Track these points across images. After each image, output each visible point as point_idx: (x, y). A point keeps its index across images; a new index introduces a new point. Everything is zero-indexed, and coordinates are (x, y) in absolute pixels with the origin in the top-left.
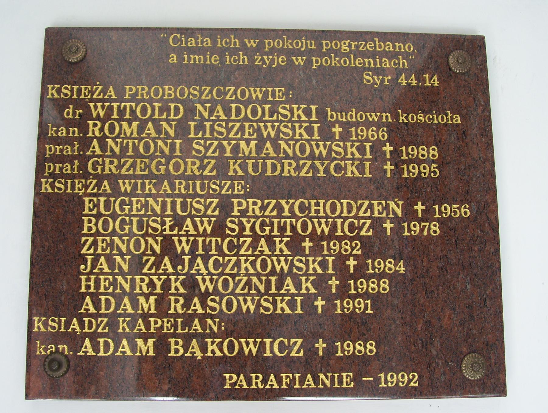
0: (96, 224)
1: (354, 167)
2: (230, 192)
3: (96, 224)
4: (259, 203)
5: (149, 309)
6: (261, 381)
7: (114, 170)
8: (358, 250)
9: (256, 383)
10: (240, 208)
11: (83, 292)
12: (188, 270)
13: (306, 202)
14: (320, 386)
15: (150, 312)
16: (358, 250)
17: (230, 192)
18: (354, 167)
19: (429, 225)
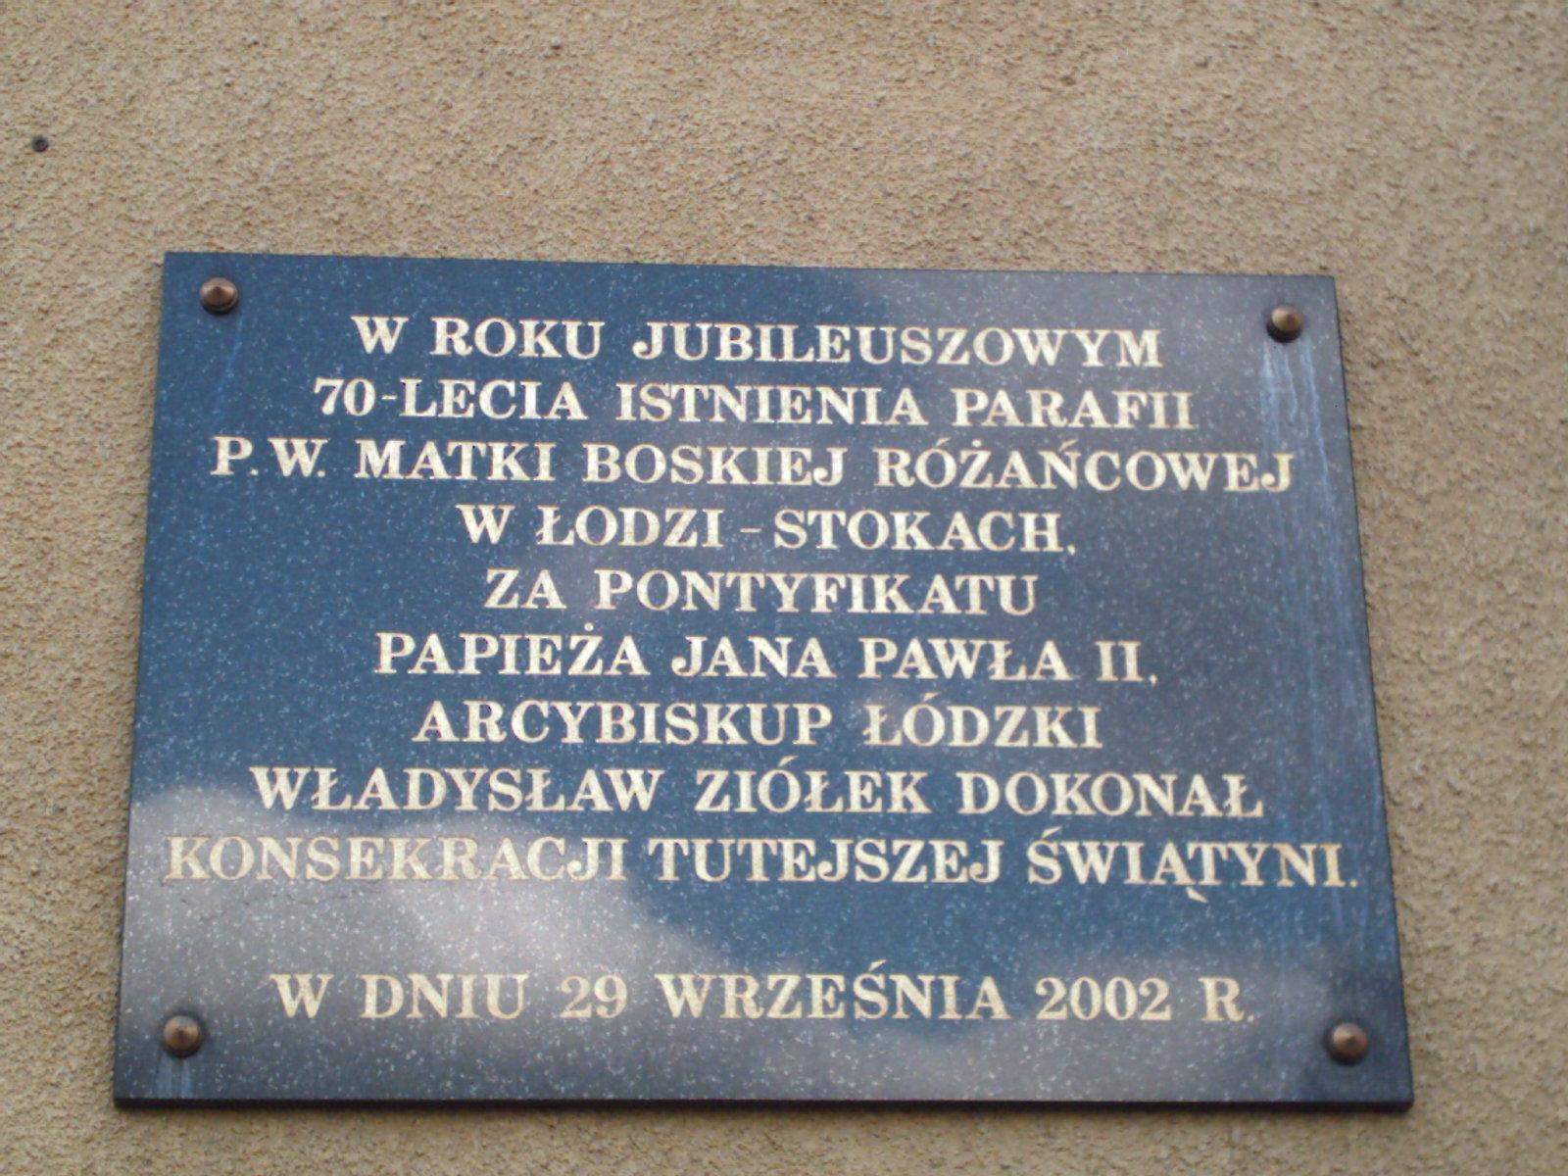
0: (621, 462)
1: (730, 463)
2: (797, 1013)
3: (621, 462)
4: (753, 985)
5: (1145, 357)
6: (498, 723)
7: (468, 870)
8: (1160, 1008)
9: (483, 729)
10: (615, 591)
11: (509, 676)
12: (210, 849)
13: (511, 386)
14: (758, 673)
15: (1146, 365)
16: (1160, 1008)
17: (797, 1013)
18: (730, 463)
19: (344, 388)
